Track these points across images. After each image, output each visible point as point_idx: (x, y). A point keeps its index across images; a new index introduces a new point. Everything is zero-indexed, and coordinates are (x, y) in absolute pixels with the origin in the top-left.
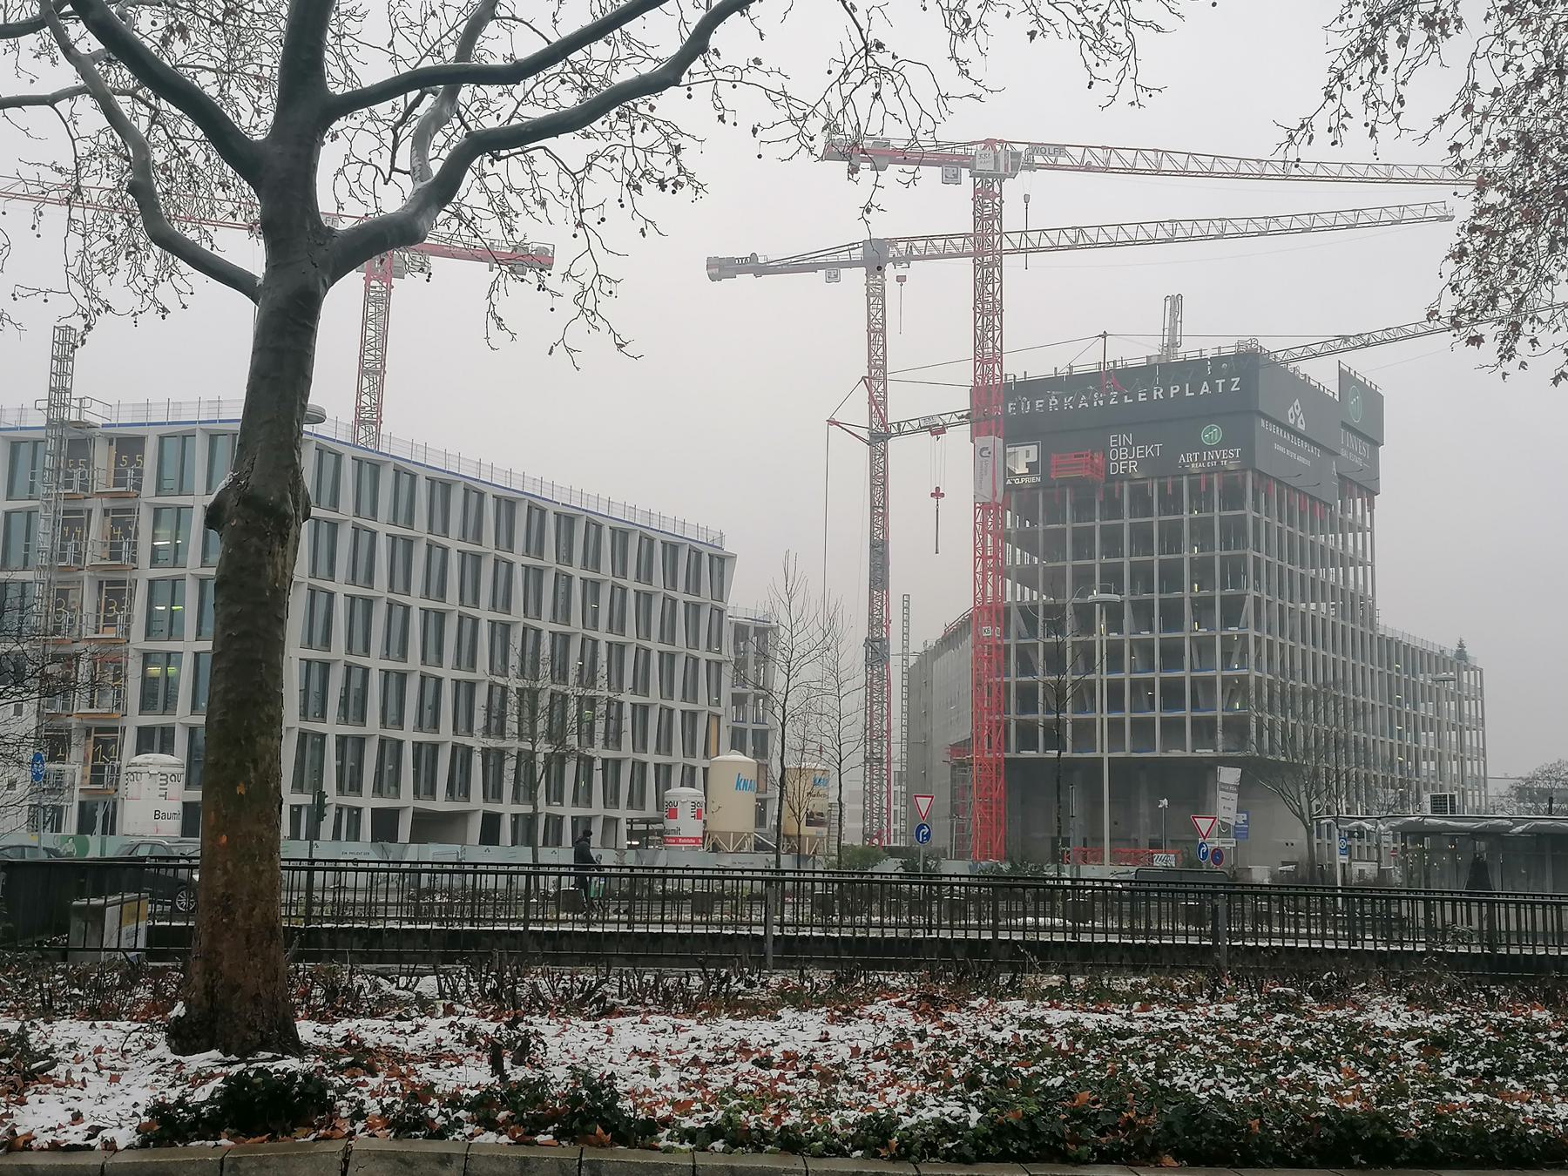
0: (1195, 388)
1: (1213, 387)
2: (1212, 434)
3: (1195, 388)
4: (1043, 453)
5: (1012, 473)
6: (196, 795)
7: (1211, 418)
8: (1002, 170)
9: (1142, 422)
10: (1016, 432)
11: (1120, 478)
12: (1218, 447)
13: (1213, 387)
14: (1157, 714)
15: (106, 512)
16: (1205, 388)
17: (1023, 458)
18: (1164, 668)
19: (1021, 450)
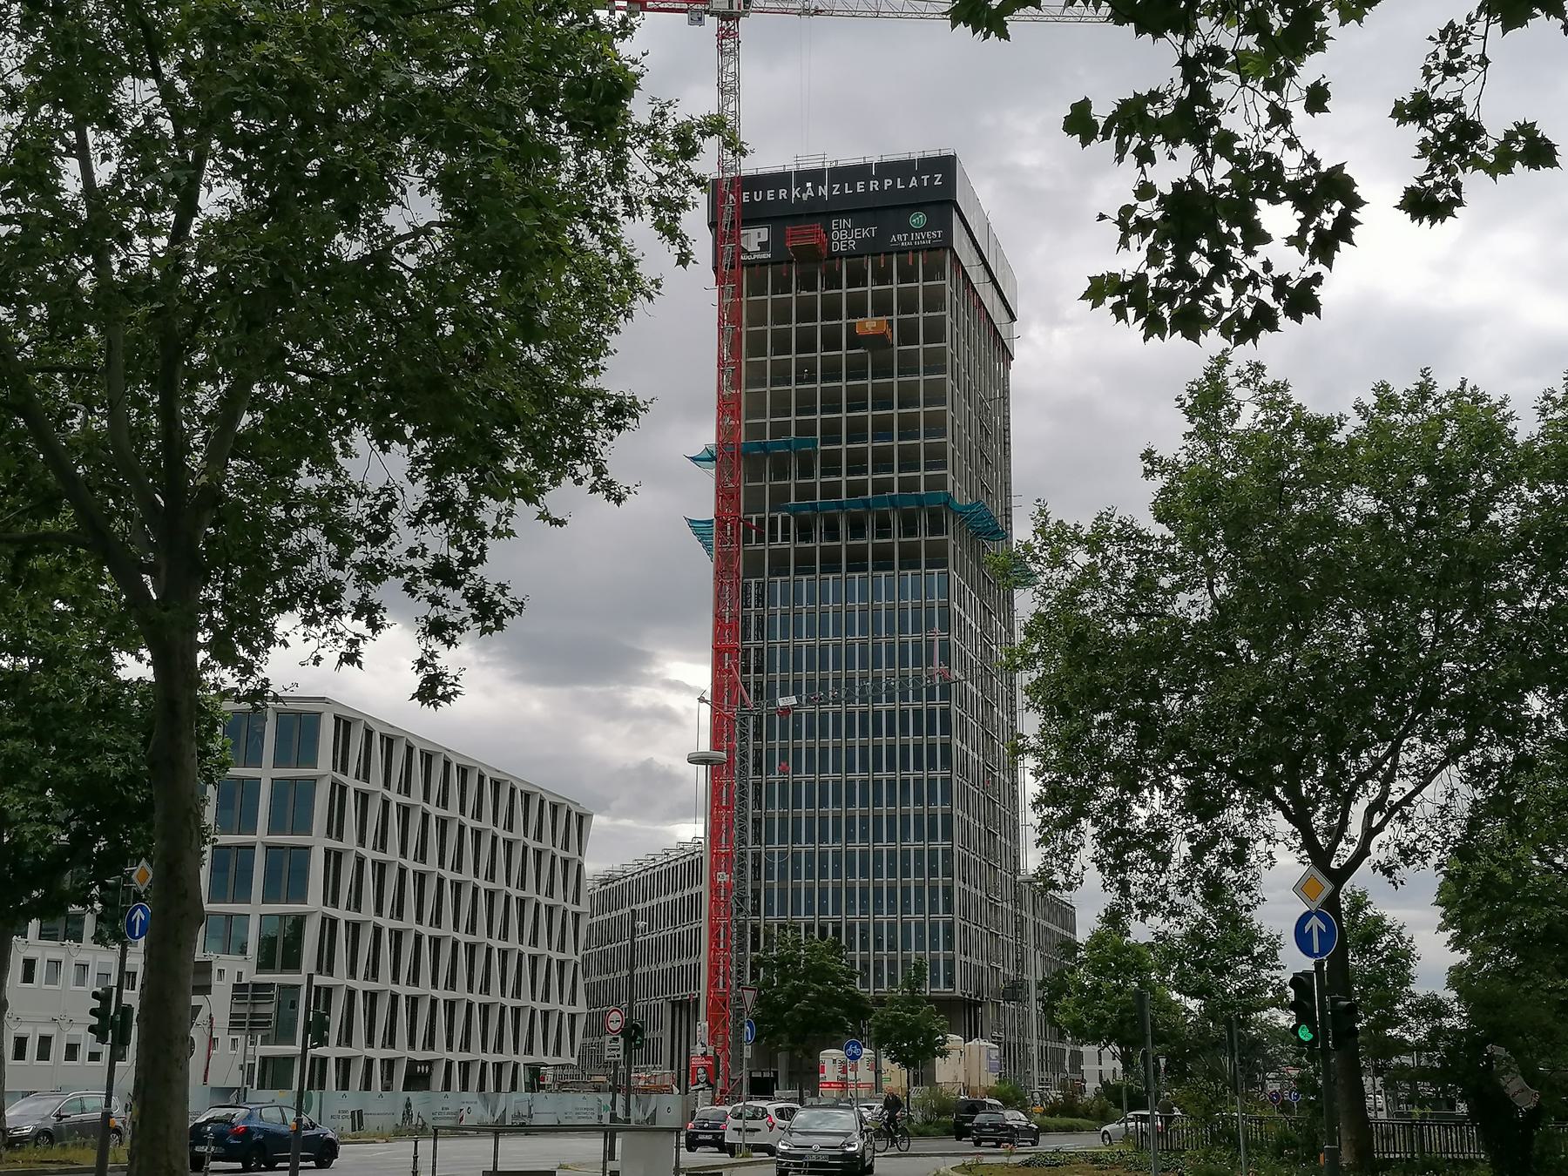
0: (906, 182)
1: (920, 181)
2: (917, 219)
3: (906, 182)
4: (774, 235)
5: (745, 251)
6: (196, 1000)
7: (918, 207)
8: (735, 9)
9: (860, 211)
10: (751, 216)
11: (840, 255)
12: (923, 230)
13: (920, 181)
14: (844, 478)
15: (239, 988)
16: (913, 182)
17: (754, 239)
18: (824, 473)
19: (753, 232)
